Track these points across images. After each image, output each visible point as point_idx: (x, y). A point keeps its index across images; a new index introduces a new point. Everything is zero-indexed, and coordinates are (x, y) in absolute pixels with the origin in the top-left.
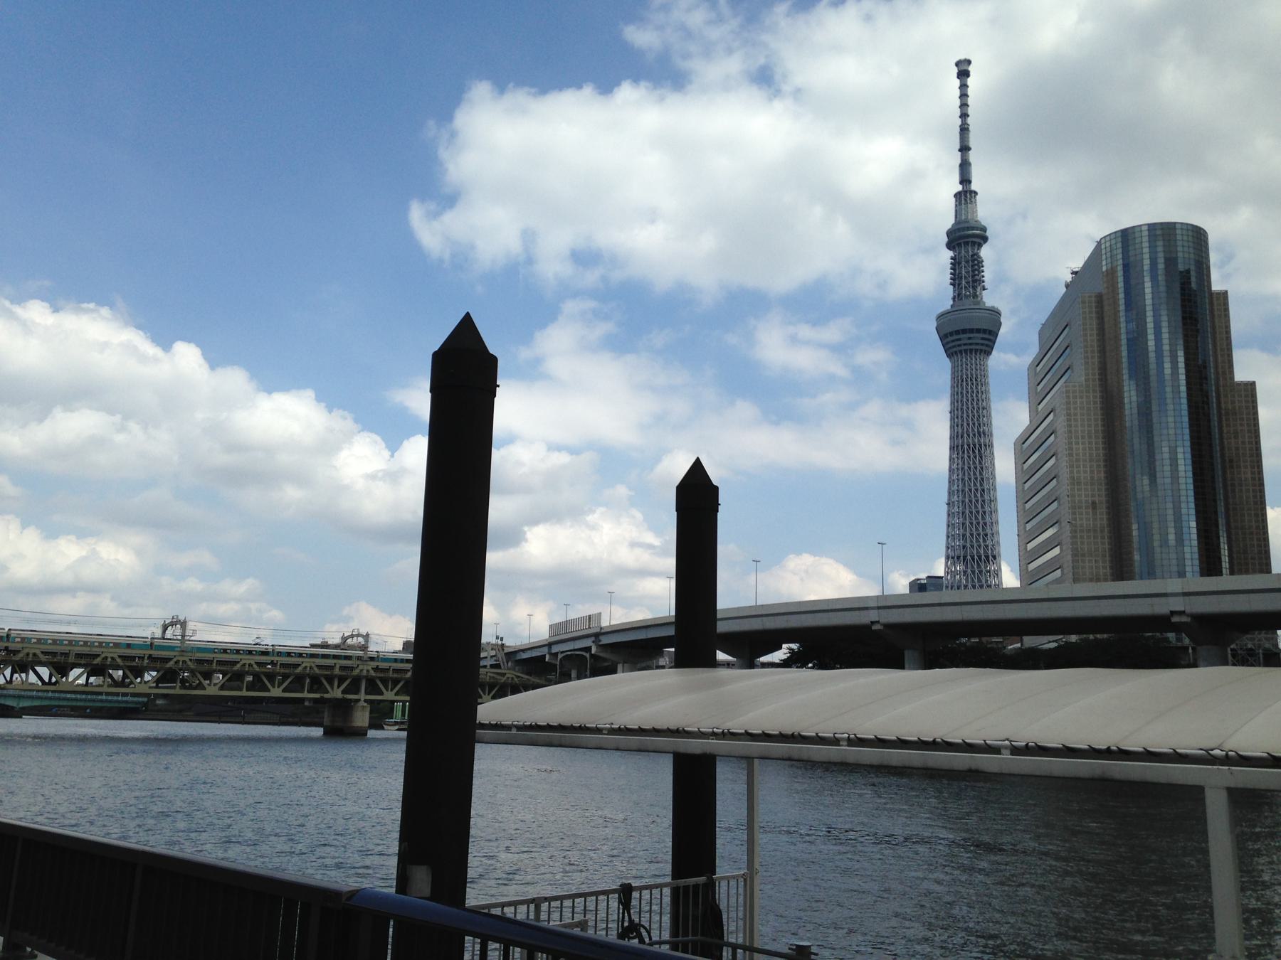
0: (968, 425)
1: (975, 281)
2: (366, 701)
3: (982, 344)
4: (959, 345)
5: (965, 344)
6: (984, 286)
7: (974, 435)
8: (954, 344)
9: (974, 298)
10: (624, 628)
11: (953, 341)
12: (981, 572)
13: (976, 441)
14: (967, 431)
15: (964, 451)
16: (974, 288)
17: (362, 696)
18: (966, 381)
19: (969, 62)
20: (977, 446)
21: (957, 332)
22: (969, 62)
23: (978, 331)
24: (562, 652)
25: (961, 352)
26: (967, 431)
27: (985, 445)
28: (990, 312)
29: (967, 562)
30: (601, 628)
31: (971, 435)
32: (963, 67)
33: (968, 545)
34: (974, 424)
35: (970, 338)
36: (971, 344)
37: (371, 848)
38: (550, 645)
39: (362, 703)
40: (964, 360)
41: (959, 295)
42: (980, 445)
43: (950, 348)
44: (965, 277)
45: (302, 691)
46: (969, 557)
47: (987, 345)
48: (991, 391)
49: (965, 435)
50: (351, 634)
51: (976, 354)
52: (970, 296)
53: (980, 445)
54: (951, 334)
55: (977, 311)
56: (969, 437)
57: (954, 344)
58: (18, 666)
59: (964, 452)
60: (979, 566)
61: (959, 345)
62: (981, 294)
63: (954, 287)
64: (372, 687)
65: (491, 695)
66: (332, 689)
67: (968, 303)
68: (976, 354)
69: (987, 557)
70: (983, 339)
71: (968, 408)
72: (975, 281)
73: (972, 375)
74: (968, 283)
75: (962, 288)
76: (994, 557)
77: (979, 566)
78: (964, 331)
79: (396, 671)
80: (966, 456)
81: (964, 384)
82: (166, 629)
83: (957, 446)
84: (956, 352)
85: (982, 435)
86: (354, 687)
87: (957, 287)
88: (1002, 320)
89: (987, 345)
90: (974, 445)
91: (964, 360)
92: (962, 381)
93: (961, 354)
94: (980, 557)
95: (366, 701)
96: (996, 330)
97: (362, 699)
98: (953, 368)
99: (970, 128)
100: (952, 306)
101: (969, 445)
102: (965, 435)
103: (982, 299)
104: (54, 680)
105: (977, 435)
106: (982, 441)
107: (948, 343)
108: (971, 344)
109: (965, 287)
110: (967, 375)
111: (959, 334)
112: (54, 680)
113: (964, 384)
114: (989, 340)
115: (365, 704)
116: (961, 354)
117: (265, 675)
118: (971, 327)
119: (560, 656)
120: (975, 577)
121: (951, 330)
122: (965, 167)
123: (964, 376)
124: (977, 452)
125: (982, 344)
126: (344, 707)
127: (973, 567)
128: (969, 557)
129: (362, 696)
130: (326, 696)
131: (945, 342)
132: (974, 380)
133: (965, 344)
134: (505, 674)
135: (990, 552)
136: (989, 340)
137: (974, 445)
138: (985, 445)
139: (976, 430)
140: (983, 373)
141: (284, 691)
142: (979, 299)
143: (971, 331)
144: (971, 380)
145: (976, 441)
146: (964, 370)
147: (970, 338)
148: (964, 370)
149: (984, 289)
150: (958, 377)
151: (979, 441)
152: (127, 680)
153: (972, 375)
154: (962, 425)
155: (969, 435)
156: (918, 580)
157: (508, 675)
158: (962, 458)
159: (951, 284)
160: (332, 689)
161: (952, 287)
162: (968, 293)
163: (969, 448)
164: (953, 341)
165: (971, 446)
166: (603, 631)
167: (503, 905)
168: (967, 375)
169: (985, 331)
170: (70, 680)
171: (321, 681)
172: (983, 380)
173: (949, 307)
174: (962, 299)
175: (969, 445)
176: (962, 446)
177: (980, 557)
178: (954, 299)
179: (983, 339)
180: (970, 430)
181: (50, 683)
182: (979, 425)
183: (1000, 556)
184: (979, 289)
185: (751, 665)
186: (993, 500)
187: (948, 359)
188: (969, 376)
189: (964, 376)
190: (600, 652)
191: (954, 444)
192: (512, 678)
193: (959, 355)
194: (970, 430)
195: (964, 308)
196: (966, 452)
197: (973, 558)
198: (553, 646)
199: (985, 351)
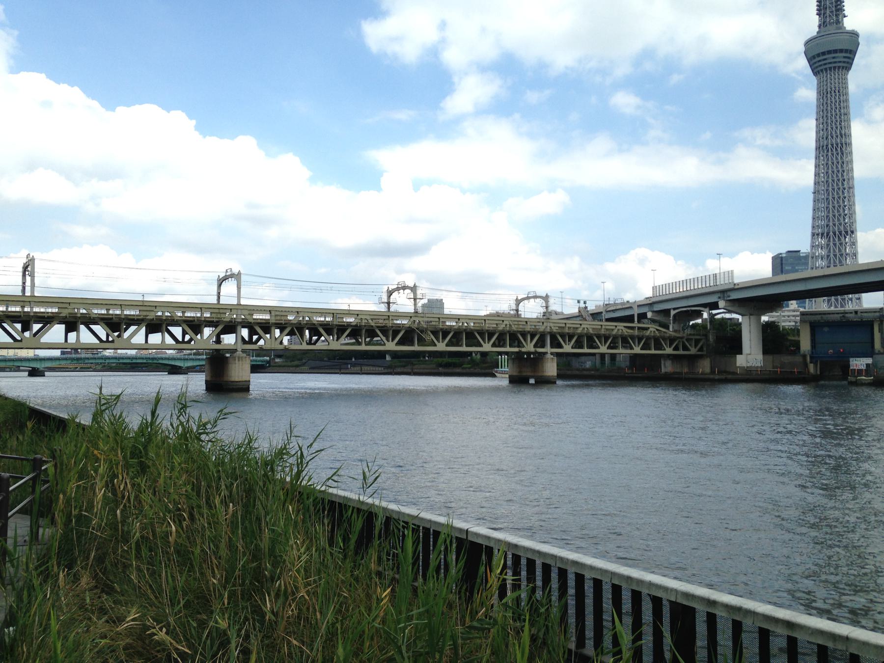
0: (832, 128)
1: (837, 10)
2: (552, 354)
3: (844, 62)
4: (825, 64)
5: (830, 63)
6: (844, 14)
7: (837, 136)
8: (820, 63)
9: (836, 24)
10: (751, 285)
11: (819, 61)
12: (841, 244)
13: (839, 141)
14: (831, 133)
16: (837, 16)
17: (548, 349)
18: (831, 92)
20: (839, 145)
21: (823, 53)
23: (841, 51)
24: (674, 309)
25: (826, 69)
26: (831, 133)
28: (851, 35)
30: (735, 285)
31: (834, 136)
33: (831, 224)
34: (837, 128)
35: (834, 58)
36: (835, 62)
37: (504, 468)
38: (651, 305)
39: (549, 356)
40: (829, 75)
41: (824, 23)
43: (817, 67)
44: (829, 7)
45: (461, 346)
46: (831, 233)
47: (848, 63)
49: (830, 137)
50: (526, 296)
51: (839, 70)
52: (833, 23)
54: (818, 55)
55: (841, 34)
57: (820, 63)
58: (296, 328)
59: (828, 151)
60: (839, 239)
61: (825, 64)
62: (842, 20)
63: (820, 17)
64: (556, 344)
65: (640, 346)
66: (527, 344)
67: (832, 29)
68: (839, 70)
69: (847, 232)
70: (845, 57)
71: (832, 115)
72: (837, 10)
73: (835, 88)
74: (832, 12)
75: (826, 17)
76: (852, 232)
77: (839, 239)
78: (829, 52)
79: (574, 328)
81: (829, 95)
82: (391, 294)
83: (823, 147)
84: (822, 71)
85: (843, 136)
86: (541, 343)
87: (822, 16)
88: (859, 41)
89: (848, 63)
90: (837, 144)
91: (829, 75)
92: (827, 93)
93: (826, 72)
94: (840, 233)
95: (552, 354)
96: (855, 50)
97: (549, 352)
100: (818, 33)
101: (832, 145)
102: (830, 137)
103: (843, 24)
104: (187, 338)
105: (839, 136)
106: (843, 141)
107: (814, 69)
108: (835, 62)
109: (830, 16)
110: (831, 88)
111: (837, 53)
112: (110, 339)
113: (829, 95)
114: (849, 58)
115: (552, 356)
116: (826, 72)
117: (478, 333)
118: (835, 49)
119: (673, 313)
121: (817, 53)
123: (829, 89)
124: (839, 149)
125: (844, 62)
126: (536, 360)
127: (834, 240)
128: (831, 233)
129: (548, 349)
130: (523, 350)
131: (812, 63)
132: (837, 91)
133: (830, 63)
134: (649, 328)
135: (849, 229)
136: (849, 58)
137: (837, 144)
138: (846, 144)
139: (838, 133)
140: (844, 86)
141: (397, 344)
142: (841, 24)
143: (835, 51)
144: (835, 92)
145: (839, 141)
146: (829, 84)
147: (834, 58)
148: (829, 84)
149: (845, 17)
151: (841, 141)
152: (255, 337)
153: (835, 88)
154: (827, 129)
155: (832, 137)
156: (781, 254)
157: (651, 329)
158: (827, 155)
159: (817, 14)
160: (527, 344)
161: (818, 16)
162: (832, 21)
163: (833, 147)
164: (819, 61)
165: (835, 145)
166: (736, 287)
168: (831, 88)
169: (846, 51)
170: (205, 338)
171: (557, 337)
172: (844, 91)
173: (816, 34)
174: (827, 25)
175: (832, 145)
176: (827, 146)
177: (840, 233)
178: (820, 26)
179: (845, 57)
180: (834, 133)
181: (183, 342)
182: (841, 128)
183: (856, 230)
184: (840, 17)
186: (851, 188)
187: (814, 77)
188: (833, 89)
189: (829, 89)
190: (728, 306)
191: (820, 145)
192: (654, 332)
193: (824, 72)
194: (834, 133)
195: (830, 32)
197: (835, 234)
199: (846, 67)
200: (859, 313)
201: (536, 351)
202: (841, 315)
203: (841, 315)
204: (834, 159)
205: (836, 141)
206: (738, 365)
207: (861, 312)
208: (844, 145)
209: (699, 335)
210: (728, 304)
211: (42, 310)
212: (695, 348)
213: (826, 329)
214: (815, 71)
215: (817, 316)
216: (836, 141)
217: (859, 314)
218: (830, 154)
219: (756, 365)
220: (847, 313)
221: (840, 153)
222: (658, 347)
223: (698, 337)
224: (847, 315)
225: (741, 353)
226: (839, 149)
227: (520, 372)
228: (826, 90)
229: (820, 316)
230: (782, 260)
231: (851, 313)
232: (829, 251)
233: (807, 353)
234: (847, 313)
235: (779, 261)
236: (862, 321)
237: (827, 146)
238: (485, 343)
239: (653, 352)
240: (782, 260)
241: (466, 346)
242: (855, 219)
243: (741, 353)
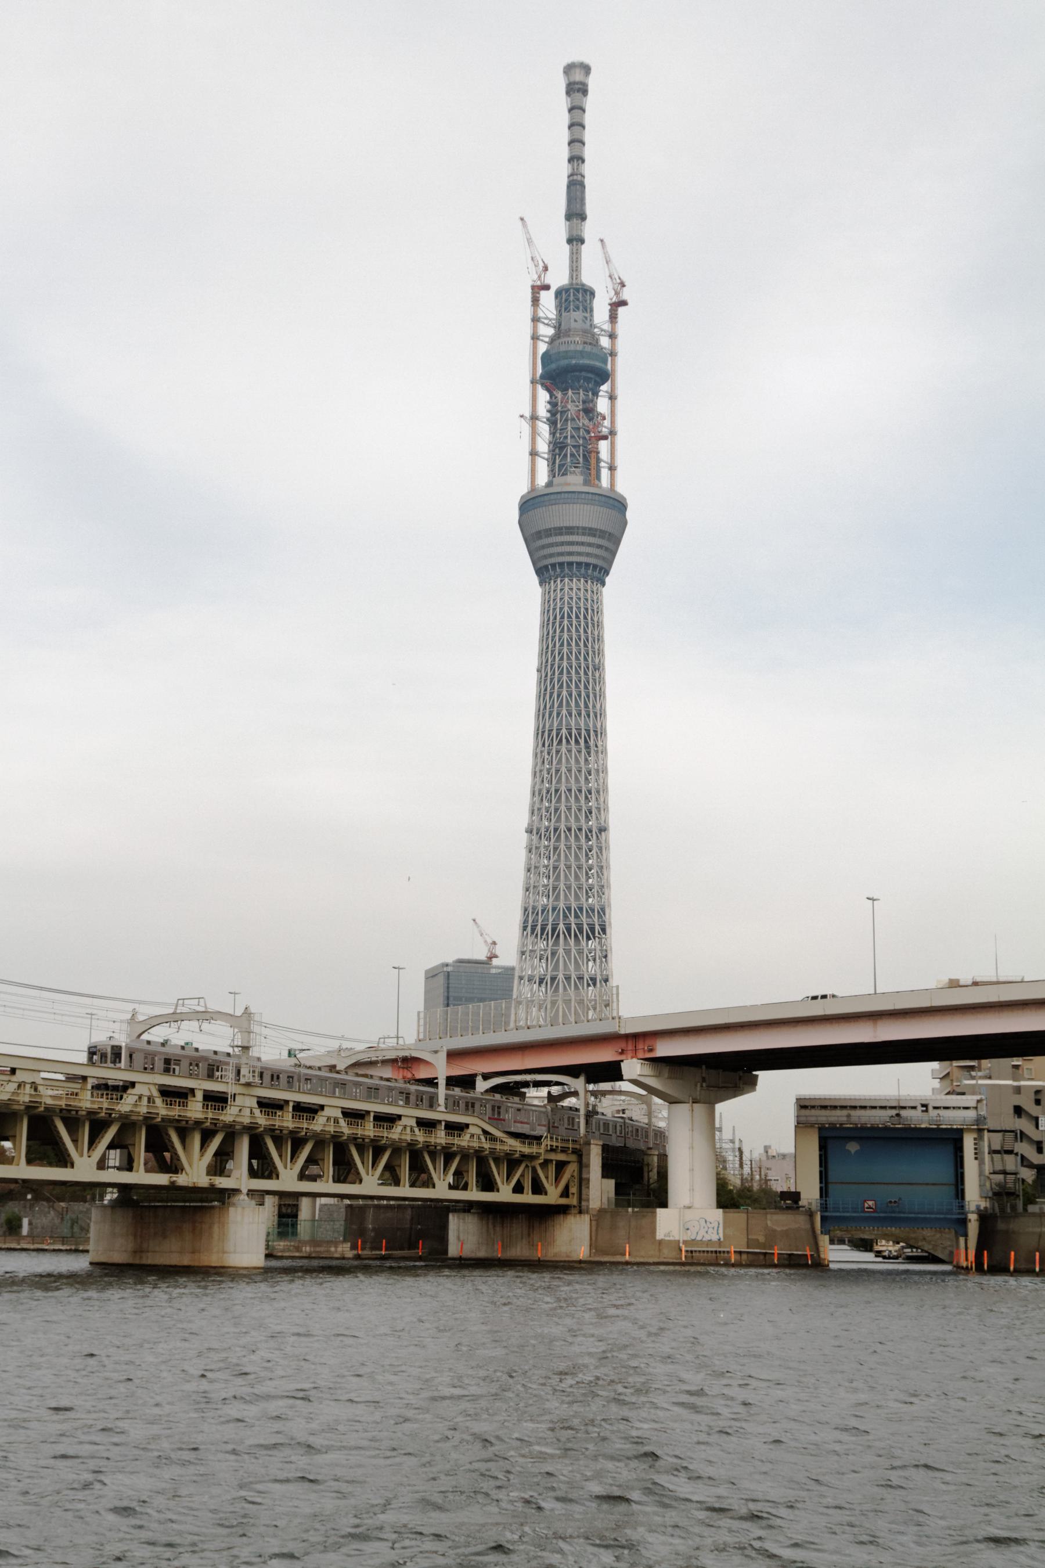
15: (559, 817)
19: (586, 69)
20: (583, 732)
22: (586, 69)
24: (486, 1077)
27: (596, 732)
29: (558, 935)
32: (578, 76)
42: (588, 731)
48: (605, 611)
53: (588, 731)
56: (571, 715)
73: (579, 608)
80: (561, 951)
90: (579, 730)
97: (245, 1191)
98: (544, 594)
99: (587, 182)
110: (571, 608)
120: (570, 854)
122: (576, 125)
124: (582, 742)
145: (573, 724)
150: (554, 609)
151: (586, 724)
153: (579, 608)
167: (535, 338)
176: (559, 730)
185: (533, 382)
196: (564, 740)
198: (541, 314)
200: (930, 1108)
201: (212, 1185)
202: (894, 1112)
203: (894, 1112)
204: (573, 762)
205: (577, 723)
206: (660, 1235)
207: (935, 1108)
208: (592, 733)
209: (564, 1150)
210: (647, 1070)
211: (588, 362)
212: (556, 1187)
213: (853, 1147)
214: (541, 564)
215: (838, 1112)
216: (577, 723)
217: (933, 1113)
218: (564, 749)
219: (707, 1238)
220: (904, 1108)
221: (584, 751)
222: (420, 1175)
223: (562, 1157)
224: (903, 1113)
225: (664, 1205)
226: (582, 742)
227: (138, 1251)
228: (561, 609)
229: (845, 1112)
230: (448, 976)
231: (914, 1108)
232: (556, 967)
233: (814, 1207)
234: (904, 1108)
235: (441, 980)
236: (939, 1130)
237: (559, 730)
238: (82, 1155)
239: (405, 1191)
240: (448, 976)
241: (30, 1161)
242: (609, 899)
243: (664, 1205)
